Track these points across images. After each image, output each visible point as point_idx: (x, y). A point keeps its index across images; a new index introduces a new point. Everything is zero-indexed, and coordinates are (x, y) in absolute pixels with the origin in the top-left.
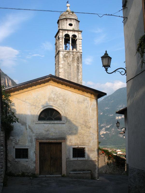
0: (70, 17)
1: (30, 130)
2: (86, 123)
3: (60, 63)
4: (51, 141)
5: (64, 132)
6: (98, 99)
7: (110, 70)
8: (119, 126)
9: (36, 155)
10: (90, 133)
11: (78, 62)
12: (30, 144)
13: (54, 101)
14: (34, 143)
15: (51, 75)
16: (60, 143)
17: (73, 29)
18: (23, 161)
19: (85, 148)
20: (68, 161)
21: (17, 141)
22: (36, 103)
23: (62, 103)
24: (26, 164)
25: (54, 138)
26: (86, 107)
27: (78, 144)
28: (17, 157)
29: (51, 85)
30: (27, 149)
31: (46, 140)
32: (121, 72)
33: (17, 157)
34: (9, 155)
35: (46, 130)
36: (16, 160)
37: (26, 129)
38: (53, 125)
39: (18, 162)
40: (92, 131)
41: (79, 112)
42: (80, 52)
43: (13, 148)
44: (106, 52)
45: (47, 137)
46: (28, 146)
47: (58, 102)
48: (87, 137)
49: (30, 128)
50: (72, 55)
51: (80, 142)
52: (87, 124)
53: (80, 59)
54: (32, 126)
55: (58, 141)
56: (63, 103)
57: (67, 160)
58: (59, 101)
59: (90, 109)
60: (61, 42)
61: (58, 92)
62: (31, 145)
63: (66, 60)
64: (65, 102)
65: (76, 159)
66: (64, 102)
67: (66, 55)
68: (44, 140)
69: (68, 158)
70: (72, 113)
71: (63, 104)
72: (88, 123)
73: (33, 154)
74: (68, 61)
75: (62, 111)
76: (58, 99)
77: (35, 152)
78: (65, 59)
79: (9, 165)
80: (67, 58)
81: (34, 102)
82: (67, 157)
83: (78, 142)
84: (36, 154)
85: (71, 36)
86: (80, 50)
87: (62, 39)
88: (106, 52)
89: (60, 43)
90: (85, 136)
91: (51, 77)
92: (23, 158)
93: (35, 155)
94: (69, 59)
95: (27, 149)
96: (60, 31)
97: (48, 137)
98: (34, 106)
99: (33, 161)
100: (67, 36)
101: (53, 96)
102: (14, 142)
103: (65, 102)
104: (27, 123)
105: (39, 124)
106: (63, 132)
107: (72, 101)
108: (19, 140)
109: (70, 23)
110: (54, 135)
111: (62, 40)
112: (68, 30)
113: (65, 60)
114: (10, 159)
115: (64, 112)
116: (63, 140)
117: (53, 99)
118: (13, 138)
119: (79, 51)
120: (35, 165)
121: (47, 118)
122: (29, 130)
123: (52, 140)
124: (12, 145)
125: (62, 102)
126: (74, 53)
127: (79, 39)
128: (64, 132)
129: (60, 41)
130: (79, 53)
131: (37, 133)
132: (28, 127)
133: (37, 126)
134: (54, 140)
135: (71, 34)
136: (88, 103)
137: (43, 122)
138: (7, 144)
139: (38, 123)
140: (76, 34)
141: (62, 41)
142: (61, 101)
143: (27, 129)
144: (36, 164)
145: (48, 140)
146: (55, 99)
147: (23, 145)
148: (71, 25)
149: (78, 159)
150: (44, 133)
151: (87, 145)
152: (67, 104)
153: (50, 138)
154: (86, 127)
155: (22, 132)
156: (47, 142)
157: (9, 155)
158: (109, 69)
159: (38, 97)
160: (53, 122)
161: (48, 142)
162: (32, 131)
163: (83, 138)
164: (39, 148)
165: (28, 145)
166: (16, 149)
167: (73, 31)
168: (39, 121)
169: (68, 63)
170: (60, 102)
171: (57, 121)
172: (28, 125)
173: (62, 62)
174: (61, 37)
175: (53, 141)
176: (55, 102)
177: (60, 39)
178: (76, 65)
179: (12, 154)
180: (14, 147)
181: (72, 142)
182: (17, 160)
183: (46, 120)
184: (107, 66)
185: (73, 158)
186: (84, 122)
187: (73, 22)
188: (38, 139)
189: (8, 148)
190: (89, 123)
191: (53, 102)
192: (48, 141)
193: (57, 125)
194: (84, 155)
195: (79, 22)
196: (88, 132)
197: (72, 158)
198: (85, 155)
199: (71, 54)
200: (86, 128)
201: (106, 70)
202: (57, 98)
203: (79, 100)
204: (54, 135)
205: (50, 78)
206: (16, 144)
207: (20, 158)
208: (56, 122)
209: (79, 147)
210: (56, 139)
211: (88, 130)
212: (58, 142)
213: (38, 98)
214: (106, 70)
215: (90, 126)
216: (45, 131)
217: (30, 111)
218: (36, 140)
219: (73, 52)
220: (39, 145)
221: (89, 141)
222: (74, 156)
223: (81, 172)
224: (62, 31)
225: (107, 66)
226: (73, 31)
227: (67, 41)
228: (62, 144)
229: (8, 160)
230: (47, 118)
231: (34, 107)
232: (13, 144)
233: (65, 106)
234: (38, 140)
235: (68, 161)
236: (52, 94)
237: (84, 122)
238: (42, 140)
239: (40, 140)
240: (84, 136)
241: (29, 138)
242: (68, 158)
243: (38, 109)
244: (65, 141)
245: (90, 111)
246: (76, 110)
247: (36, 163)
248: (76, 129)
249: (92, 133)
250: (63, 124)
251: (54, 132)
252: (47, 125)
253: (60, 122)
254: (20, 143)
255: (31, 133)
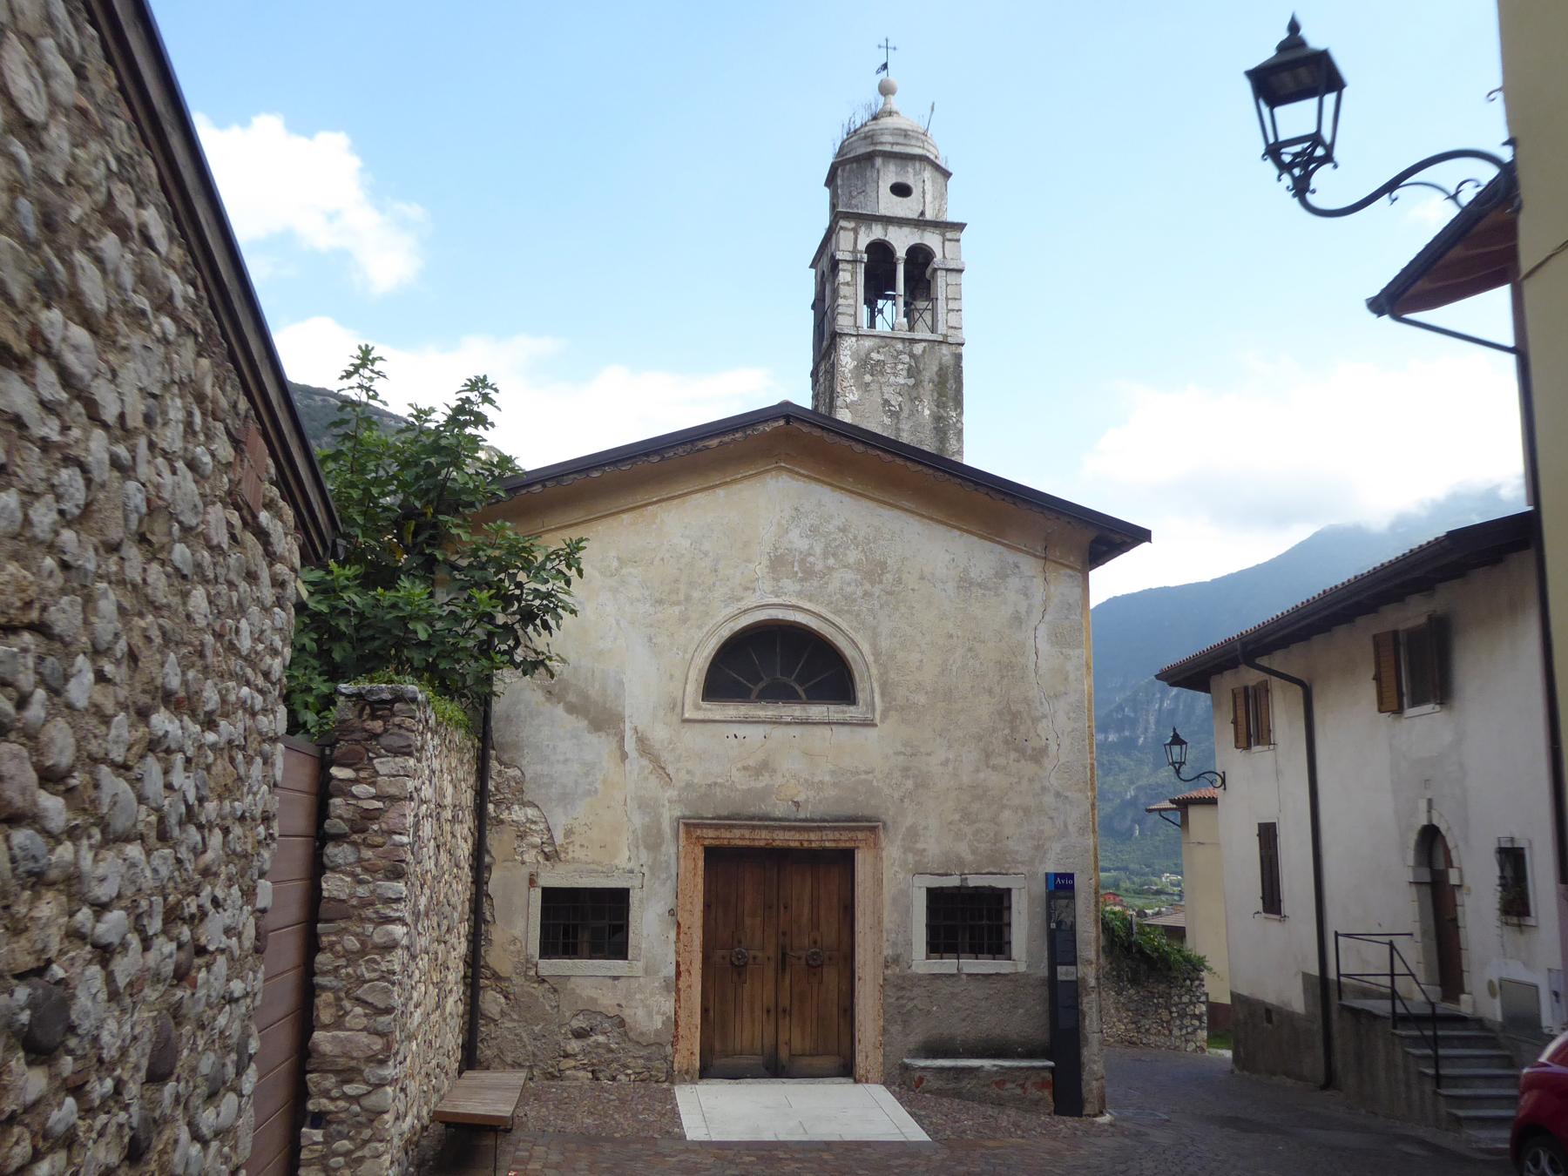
0: (897, 149)
1: (645, 762)
2: (1011, 722)
3: (839, 402)
4: (782, 839)
5: (870, 777)
6: (1092, 574)
7: (1328, 186)
8: (1181, 764)
9: (678, 934)
10: (1044, 789)
11: (940, 395)
12: (644, 856)
13: (809, 573)
14: (669, 849)
15: (787, 404)
16: (846, 858)
17: (922, 214)
18: (587, 976)
19: (1009, 890)
20: (899, 984)
21: (559, 838)
22: (691, 584)
23: (859, 593)
24: (607, 1000)
25: (802, 816)
26: (1017, 620)
27: (961, 862)
28: (548, 950)
29: (790, 471)
30: (620, 898)
31: (747, 834)
32: (1458, 193)
33: (548, 950)
34: (494, 937)
35: (751, 762)
36: (542, 972)
37: (618, 753)
38: (796, 731)
39: (555, 986)
40: (1054, 782)
41: (970, 650)
42: (950, 340)
43: (526, 883)
44: (1294, 27)
45: (753, 810)
46: (631, 872)
47: (834, 585)
48: (1021, 813)
49: (642, 741)
50: (906, 358)
51: (974, 852)
52: (1022, 729)
53: (951, 383)
54: (660, 734)
55: (828, 840)
56: (867, 586)
57: (889, 972)
58: (835, 575)
59: (1043, 631)
60: (848, 284)
61: (831, 517)
62: (651, 868)
63: (874, 387)
64: (881, 582)
65: (948, 965)
66: (873, 584)
67: (874, 355)
68: (737, 833)
69: (898, 956)
70: (922, 652)
71: (866, 594)
72: (1029, 722)
73: (660, 929)
74: (885, 389)
75: (858, 638)
76: (831, 561)
77: (672, 912)
78: (868, 378)
79: (492, 1002)
80: (882, 373)
81: (677, 581)
82: (888, 952)
83: (963, 849)
84: (679, 925)
85: (901, 253)
86: (951, 332)
87: (849, 267)
88: (1294, 27)
89: (844, 290)
90: (1007, 814)
91: (788, 423)
92: (597, 952)
93: (673, 935)
94: (892, 379)
95: (620, 898)
96: (842, 223)
97: (765, 808)
98: (678, 603)
99: (662, 975)
100: (880, 252)
101: (802, 544)
102: (534, 846)
103: (881, 582)
104: (627, 713)
105: (710, 726)
106: (863, 777)
107: (922, 578)
108: (569, 833)
109: (900, 180)
110: (807, 801)
111: (854, 274)
112: (888, 221)
113: (868, 385)
114: (498, 958)
115: (874, 646)
116: (860, 835)
117: (803, 561)
118: (530, 812)
119: (946, 336)
120: (668, 1005)
121: (761, 685)
122: (636, 763)
123: (788, 835)
124: (523, 863)
125: (859, 584)
126: (918, 349)
127: (947, 270)
128: (870, 777)
129: (844, 276)
130: (945, 350)
131: (689, 786)
132: (630, 745)
133: (694, 738)
134: (805, 836)
135: (901, 242)
136: (1026, 595)
137: (732, 710)
138: (487, 859)
139: (700, 715)
140: (932, 240)
141: (852, 282)
142: (850, 575)
143: (624, 756)
144: (677, 1000)
145: (764, 834)
146: (811, 559)
147: (593, 866)
148: (901, 190)
149: (966, 970)
150: (742, 781)
151: (1022, 869)
152: (890, 593)
153: (780, 819)
154: (1016, 750)
155: (591, 778)
156: (756, 843)
157: (497, 933)
158: (1322, 178)
159: (706, 546)
160: (797, 711)
161: (762, 843)
162: (659, 767)
163: (994, 820)
164: (701, 886)
165: (629, 866)
166: (548, 893)
167: (920, 223)
168: (705, 705)
169: (886, 402)
170: (842, 579)
171: (824, 708)
172: (636, 729)
173: (852, 396)
174: (848, 257)
175: (791, 839)
176: (815, 584)
177: (841, 266)
178: (927, 412)
179: (518, 927)
180: (532, 882)
181: (920, 846)
182: (549, 967)
183: (753, 696)
184: (1301, 163)
185: (928, 958)
186: (1000, 713)
187: (911, 175)
188: (696, 826)
189: (492, 888)
190: (1035, 720)
191: (802, 580)
192: (762, 838)
193: (826, 730)
194: (1000, 917)
195: (947, 175)
196: (1031, 780)
197: (920, 961)
198: (1009, 943)
199: (902, 352)
200: (1013, 755)
201: (1301, 189)
202: (825, 558)
203: (966, 570)
204: (801, 798)
205: (782, 423)
206: (547, 857)
207: (570, 951)
208: (817, 711)
209: (974, 881)
210: (820, 829)
211: (1029, 768)
212: (827, 844)
213: (706, 554)
214: (1301, 189)
215: (1044, 742)
216: (745, 768)
217: (650, 639)
218: (688, 833)
219: (913, 341)
220: (701, 864)
221: (1037, 848)
222: (939, 944)
223: (987, 1063)
224: (852, 225)
225: (1301, 163)
226: (920, 223)
227: (878, 284)
228: (859, 856)
229: (487, 967)
230: (761, 685)
231: (677, 609)
232: (530, 856)
233: (877, 606)
234: (699, 832)
235: (899, 984)
236: (797, 531)
237: (1000, 713)
238: (726, 834)
239: (711, 833)
240: (1004, 807)
241: (638, 820)
242: (896, 960)
243: (700, 627)
244: (877, 837)
245: (1043, 646)
246: (951, 636)
247: (678, 991)
248: (947, 760)
249: (1058, 795)
250: (868, 724)
251: (806, 781)
252: (759, 731)
253: (844, 712)
254: (576, 852)
255: (653, 782)
